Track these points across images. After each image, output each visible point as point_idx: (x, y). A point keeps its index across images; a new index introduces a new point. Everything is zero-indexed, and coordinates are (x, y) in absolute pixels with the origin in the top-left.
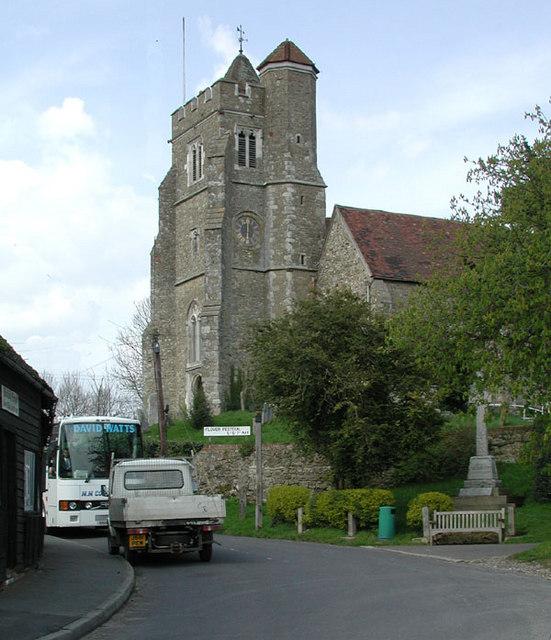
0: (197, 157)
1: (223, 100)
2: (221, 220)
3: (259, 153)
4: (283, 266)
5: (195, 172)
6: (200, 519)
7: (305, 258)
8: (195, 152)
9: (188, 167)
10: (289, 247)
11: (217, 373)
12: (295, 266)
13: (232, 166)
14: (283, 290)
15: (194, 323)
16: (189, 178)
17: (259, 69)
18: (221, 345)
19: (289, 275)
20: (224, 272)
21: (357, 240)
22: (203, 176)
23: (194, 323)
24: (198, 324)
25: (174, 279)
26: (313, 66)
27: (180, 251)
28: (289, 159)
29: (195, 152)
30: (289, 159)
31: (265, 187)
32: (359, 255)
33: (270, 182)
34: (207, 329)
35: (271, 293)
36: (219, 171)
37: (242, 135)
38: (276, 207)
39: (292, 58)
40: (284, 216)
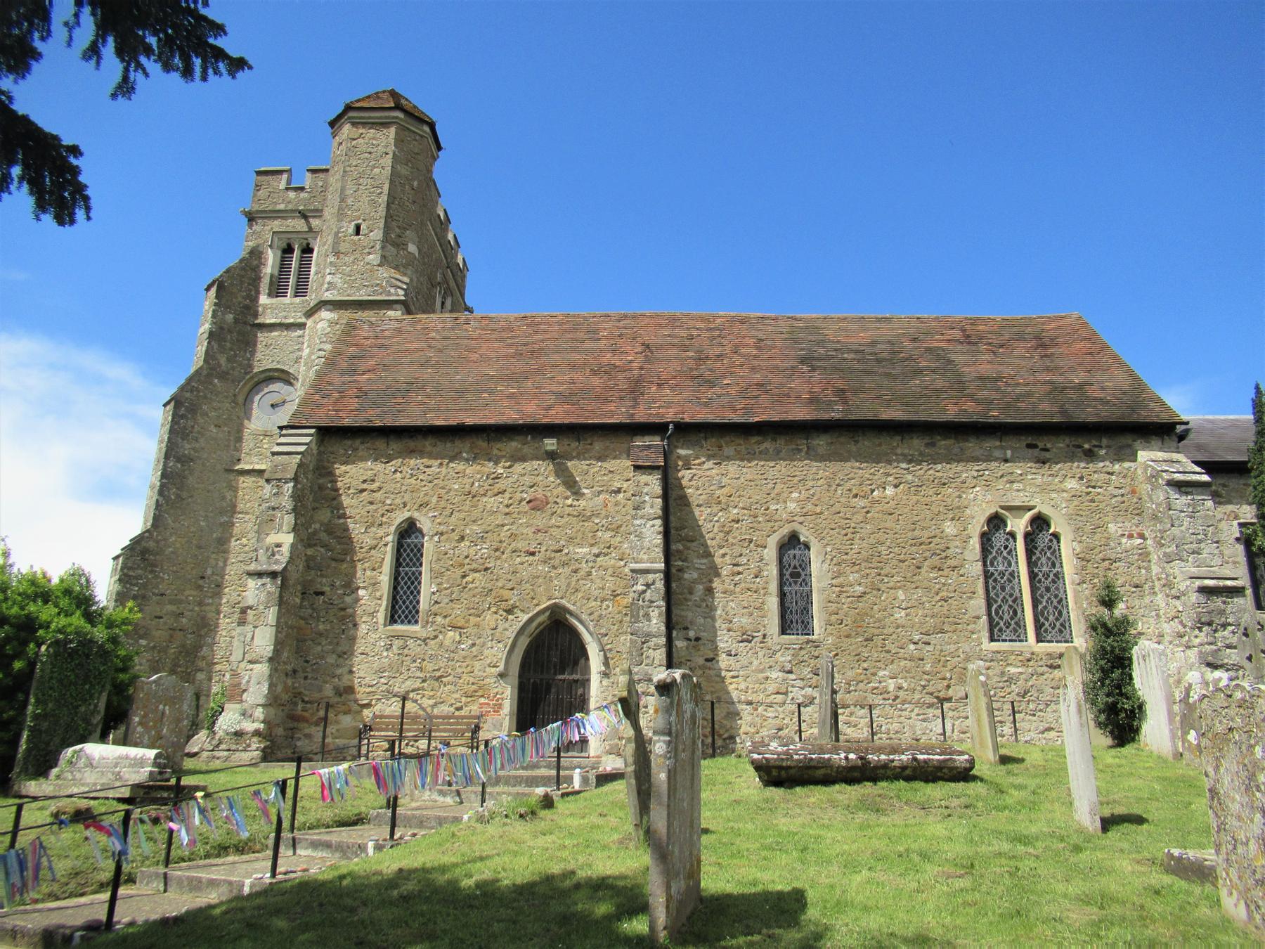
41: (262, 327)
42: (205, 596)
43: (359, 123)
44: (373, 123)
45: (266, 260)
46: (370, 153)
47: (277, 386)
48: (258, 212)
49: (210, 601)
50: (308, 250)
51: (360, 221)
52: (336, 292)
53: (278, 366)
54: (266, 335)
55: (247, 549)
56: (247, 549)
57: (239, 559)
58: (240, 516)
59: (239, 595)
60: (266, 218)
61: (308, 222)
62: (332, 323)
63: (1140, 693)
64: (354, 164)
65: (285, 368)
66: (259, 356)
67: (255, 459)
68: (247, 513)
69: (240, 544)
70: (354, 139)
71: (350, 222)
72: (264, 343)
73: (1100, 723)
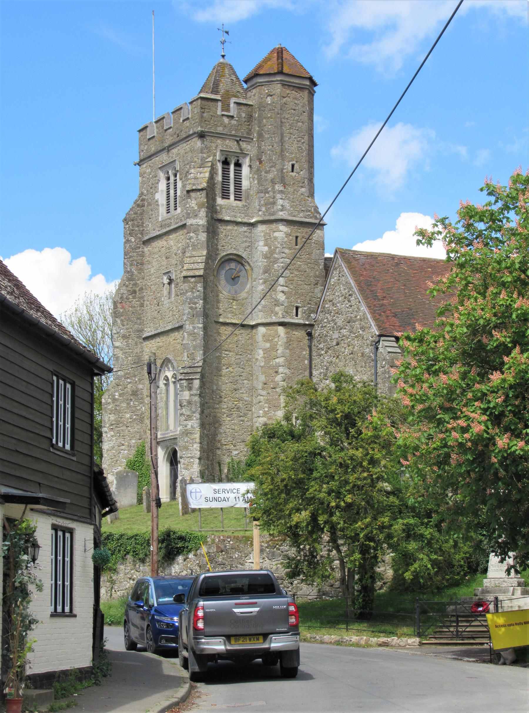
0: (172, 187)
1: (202, 120)
2: (202, 266)
3: (245, 184)
4: (274, 319)
5: (168, 204)
6: (470, 662)
7: (300, 310)
8: (168, 179)
9: (161, 197)
10: (281, 297)
11: (197, 446)
12: (287, 320)
13: (214, 200)
14: (274, 348)
15: (167, 385)
16: (162, 210)
17: (246, 82)
18: (202, 412)
19: (281, 330)
20: (205, 328)
21: (361, 290)
22: (179, 210)
23: (167, 385)
24: (172, 386)
25: (141, 331)
26: (311, 79)
27: (148, 295)
28: (281, 192)
29: (168, 179)
30: (281, 192)
31: (253, 327)
32: (364, 308)
33: (260, 321)
34: (186, 395)
35: (261, 352)
36: (201, 206)
37: (226, 163)
38: (266, 248)
39: (286, 70)
40: (276, 261)
41: (221, 221)
42: (215, 403)
43: (286, 85)
44: (294, 86)
45: (217, 170)
46: (294, 110)
47: (233, 265)
48: (208, 132)
49: (218, 406)
50: (238, 165)
51: (294, 162)
52: (287, 213)
53: (235, 252)
54: (224, 228)
55: (233, 374)
56: (233, 374)
57: (230, 380)
58: (226, 352)
59: (233, 404)
60: (212, 136)
61: (239, 144)
62: (288, 235)
63: (114, 497)
64: (286, 117)
65: (240, 253)
66: (221, 243)
67: (230, 315)
68: (230, 351)
69: (229, 371)
70: (284, 97)
71: (289, 162)
72: (224, 234)
73: (170, 532)
